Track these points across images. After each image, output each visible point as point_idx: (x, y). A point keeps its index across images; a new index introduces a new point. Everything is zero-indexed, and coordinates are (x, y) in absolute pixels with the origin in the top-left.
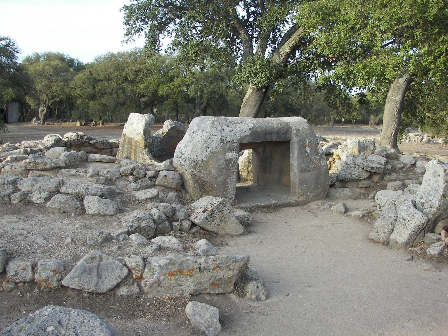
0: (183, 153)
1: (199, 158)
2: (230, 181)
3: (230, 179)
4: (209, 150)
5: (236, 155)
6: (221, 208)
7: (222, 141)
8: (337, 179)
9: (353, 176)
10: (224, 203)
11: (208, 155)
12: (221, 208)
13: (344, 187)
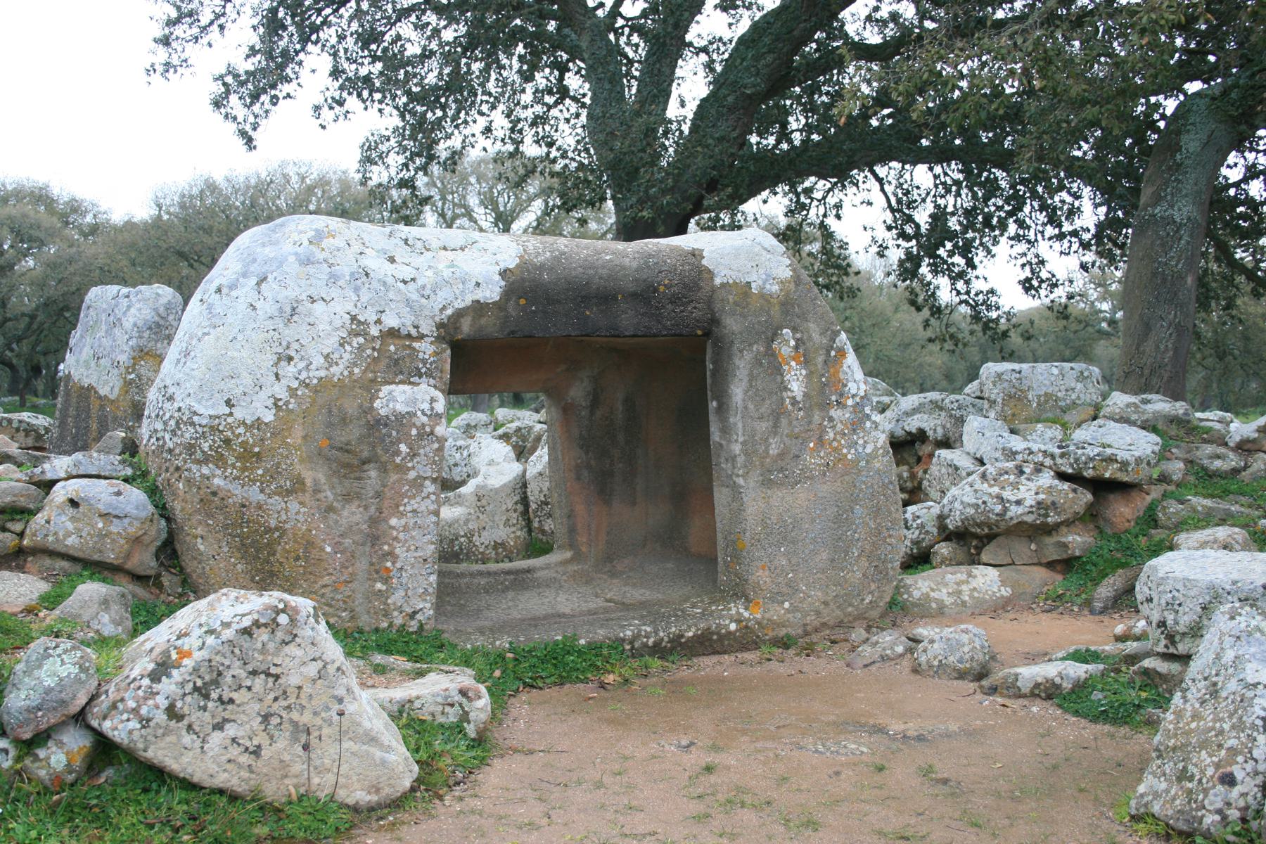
0: (171, 390)
1: (239, 413)
2: (406, 528)
3: (403, 515)
4: (289, 370)
5: (433, 400)
6: (263, 650)
7: (357, 326)
8: (942, 527)
9: (1014, 511)
10: (283, 619)
11: (283, 394)
12: (263, 650)
13: (974, 561)
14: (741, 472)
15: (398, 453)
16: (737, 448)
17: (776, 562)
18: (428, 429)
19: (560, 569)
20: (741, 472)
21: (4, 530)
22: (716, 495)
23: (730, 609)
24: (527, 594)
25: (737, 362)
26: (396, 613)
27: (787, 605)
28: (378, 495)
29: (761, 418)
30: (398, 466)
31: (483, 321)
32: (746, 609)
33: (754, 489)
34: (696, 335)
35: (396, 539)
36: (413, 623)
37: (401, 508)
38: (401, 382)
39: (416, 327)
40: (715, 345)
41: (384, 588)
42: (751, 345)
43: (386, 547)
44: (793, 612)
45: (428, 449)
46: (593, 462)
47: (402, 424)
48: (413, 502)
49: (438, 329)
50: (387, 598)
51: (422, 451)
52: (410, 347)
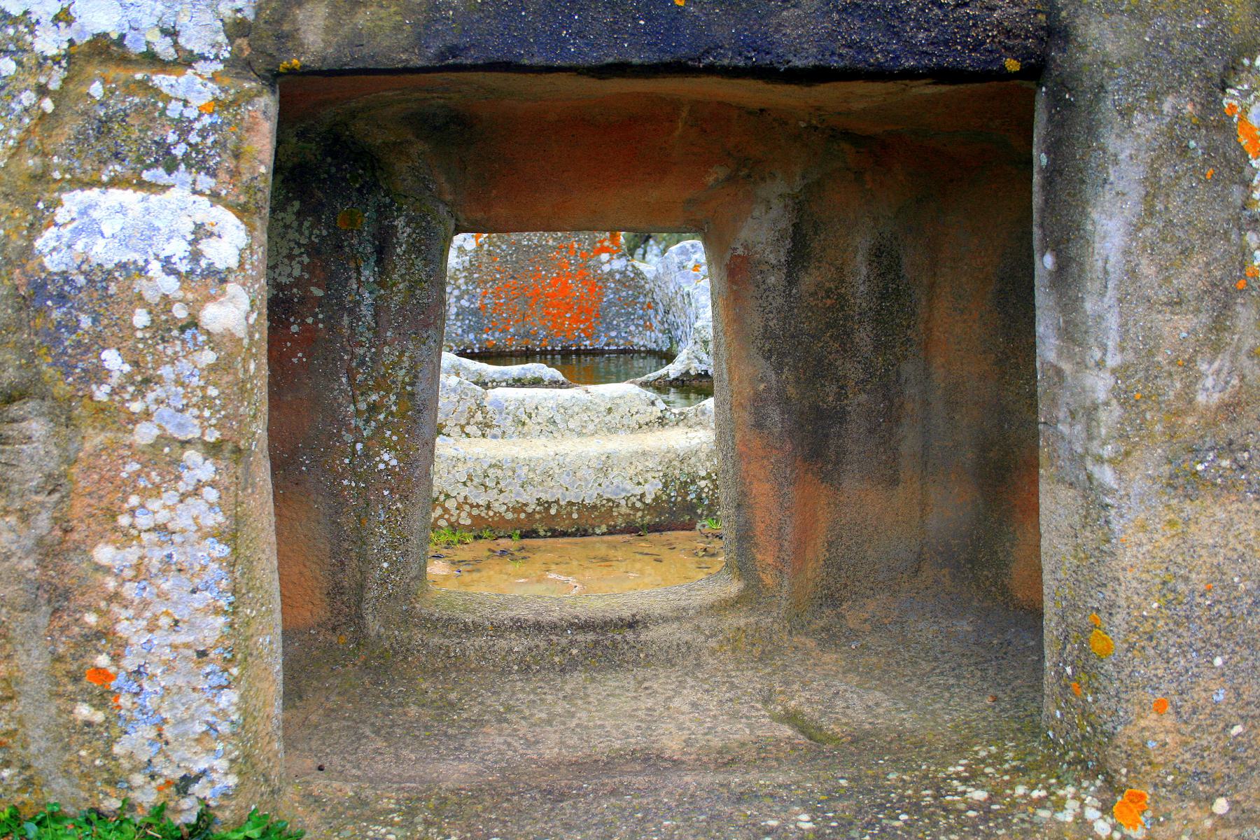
2: (140, 571)
3: (127, 537)
5: (201, 232)
14: (1108, 451)
15: (99, 374)
16: (1100, 385)
17: (1198, 695)
18: (180, 312)
19: (707, 623)
20: (1108, 451)
21: (3, 452)
22: (1045, 502)
23: (1060, 805)
24: (612, 681)
25: (1112, 142)
26: (138, 779)
27: (1221, 806)
28: (53, 484)
29: (1176, 303)
30: (101, 409)
31: (363, 18)
32: (1105, 809)
33: (1142, 497)
34: (1004, 75)
35: (115, 597)
36: (186, 803)
37: (124, 521)
38: (114, 182)
39: (171, 33)
40: (1056, 100)
41: (99, 717)
42: (1156, 96)
43: (91, 619)
44: (1238, 823)
45: (185, 366)
46: (791, 391)
47: (106, 297)
48: (154, 505)
49: (231, 38)
50: (110, 742)
51: (166, 371)
52: (144, 85)
